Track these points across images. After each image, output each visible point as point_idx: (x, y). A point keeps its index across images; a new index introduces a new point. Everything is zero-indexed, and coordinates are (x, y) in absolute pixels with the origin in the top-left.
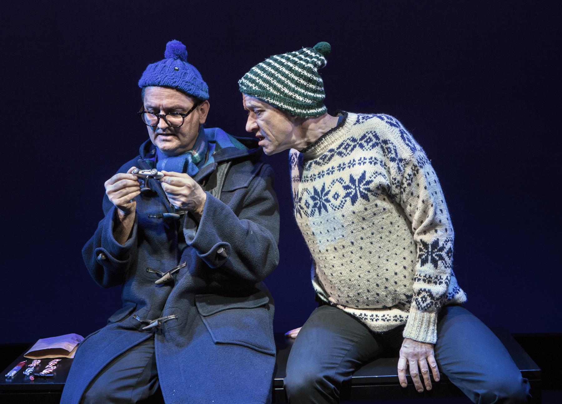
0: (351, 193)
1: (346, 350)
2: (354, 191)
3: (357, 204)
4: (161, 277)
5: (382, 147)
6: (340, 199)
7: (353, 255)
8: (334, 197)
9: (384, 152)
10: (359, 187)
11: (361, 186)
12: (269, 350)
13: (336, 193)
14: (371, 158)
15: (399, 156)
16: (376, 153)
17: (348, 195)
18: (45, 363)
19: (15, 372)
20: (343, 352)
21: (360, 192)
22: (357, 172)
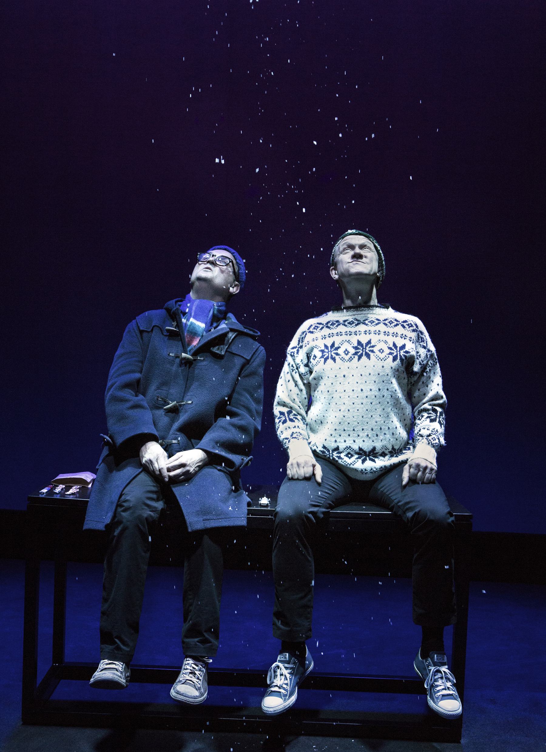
0: (358, 352)
1: (329, 494)
2: (361, 352)
3: (396, 363)
4: (169, 404)
5: (418, 335)
6: (317, 359)
7: (376, 399)
8: (347, 354)
9: (418, 339)
10: (366, 349)
11: (367, 348)
12: (397, 399)
13: (346, 350)
14: (402, 335)
15: (428, 347)
16: (414, 335)
17: (356, 354)
18: (68, 488)
19: (46, 490)
20: (327, 495)
21: (400, 355)
22: (400, 342)
